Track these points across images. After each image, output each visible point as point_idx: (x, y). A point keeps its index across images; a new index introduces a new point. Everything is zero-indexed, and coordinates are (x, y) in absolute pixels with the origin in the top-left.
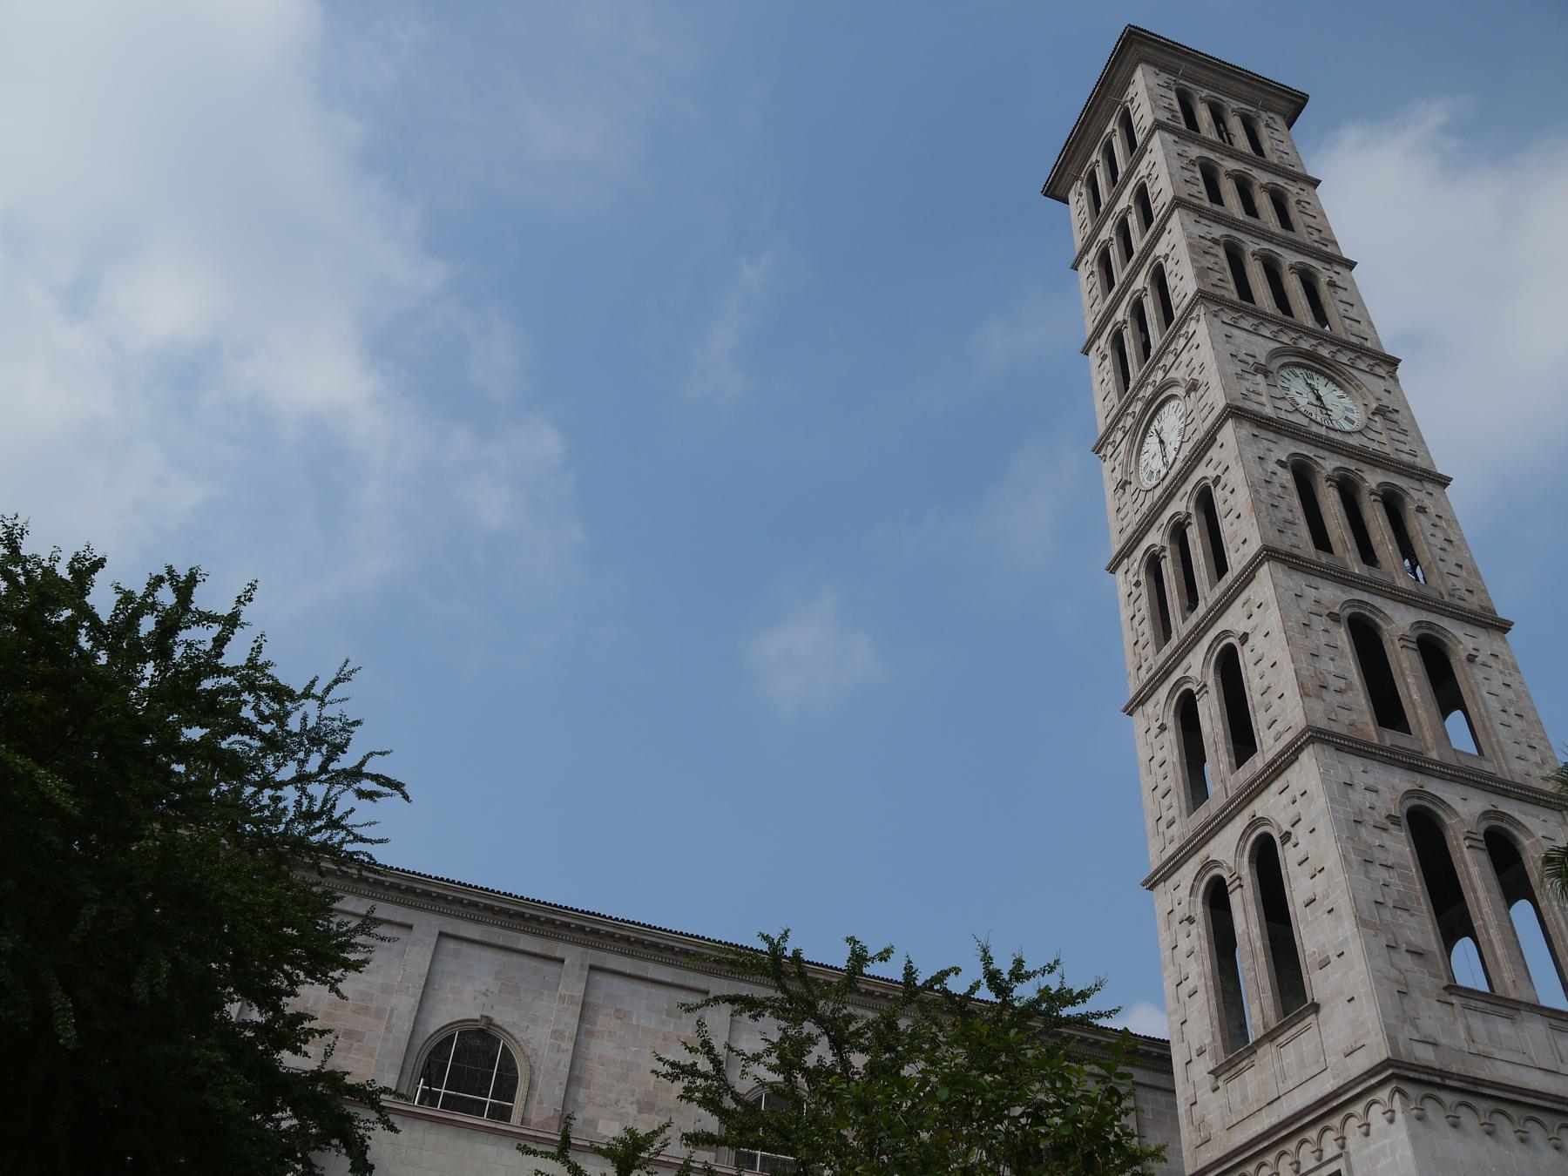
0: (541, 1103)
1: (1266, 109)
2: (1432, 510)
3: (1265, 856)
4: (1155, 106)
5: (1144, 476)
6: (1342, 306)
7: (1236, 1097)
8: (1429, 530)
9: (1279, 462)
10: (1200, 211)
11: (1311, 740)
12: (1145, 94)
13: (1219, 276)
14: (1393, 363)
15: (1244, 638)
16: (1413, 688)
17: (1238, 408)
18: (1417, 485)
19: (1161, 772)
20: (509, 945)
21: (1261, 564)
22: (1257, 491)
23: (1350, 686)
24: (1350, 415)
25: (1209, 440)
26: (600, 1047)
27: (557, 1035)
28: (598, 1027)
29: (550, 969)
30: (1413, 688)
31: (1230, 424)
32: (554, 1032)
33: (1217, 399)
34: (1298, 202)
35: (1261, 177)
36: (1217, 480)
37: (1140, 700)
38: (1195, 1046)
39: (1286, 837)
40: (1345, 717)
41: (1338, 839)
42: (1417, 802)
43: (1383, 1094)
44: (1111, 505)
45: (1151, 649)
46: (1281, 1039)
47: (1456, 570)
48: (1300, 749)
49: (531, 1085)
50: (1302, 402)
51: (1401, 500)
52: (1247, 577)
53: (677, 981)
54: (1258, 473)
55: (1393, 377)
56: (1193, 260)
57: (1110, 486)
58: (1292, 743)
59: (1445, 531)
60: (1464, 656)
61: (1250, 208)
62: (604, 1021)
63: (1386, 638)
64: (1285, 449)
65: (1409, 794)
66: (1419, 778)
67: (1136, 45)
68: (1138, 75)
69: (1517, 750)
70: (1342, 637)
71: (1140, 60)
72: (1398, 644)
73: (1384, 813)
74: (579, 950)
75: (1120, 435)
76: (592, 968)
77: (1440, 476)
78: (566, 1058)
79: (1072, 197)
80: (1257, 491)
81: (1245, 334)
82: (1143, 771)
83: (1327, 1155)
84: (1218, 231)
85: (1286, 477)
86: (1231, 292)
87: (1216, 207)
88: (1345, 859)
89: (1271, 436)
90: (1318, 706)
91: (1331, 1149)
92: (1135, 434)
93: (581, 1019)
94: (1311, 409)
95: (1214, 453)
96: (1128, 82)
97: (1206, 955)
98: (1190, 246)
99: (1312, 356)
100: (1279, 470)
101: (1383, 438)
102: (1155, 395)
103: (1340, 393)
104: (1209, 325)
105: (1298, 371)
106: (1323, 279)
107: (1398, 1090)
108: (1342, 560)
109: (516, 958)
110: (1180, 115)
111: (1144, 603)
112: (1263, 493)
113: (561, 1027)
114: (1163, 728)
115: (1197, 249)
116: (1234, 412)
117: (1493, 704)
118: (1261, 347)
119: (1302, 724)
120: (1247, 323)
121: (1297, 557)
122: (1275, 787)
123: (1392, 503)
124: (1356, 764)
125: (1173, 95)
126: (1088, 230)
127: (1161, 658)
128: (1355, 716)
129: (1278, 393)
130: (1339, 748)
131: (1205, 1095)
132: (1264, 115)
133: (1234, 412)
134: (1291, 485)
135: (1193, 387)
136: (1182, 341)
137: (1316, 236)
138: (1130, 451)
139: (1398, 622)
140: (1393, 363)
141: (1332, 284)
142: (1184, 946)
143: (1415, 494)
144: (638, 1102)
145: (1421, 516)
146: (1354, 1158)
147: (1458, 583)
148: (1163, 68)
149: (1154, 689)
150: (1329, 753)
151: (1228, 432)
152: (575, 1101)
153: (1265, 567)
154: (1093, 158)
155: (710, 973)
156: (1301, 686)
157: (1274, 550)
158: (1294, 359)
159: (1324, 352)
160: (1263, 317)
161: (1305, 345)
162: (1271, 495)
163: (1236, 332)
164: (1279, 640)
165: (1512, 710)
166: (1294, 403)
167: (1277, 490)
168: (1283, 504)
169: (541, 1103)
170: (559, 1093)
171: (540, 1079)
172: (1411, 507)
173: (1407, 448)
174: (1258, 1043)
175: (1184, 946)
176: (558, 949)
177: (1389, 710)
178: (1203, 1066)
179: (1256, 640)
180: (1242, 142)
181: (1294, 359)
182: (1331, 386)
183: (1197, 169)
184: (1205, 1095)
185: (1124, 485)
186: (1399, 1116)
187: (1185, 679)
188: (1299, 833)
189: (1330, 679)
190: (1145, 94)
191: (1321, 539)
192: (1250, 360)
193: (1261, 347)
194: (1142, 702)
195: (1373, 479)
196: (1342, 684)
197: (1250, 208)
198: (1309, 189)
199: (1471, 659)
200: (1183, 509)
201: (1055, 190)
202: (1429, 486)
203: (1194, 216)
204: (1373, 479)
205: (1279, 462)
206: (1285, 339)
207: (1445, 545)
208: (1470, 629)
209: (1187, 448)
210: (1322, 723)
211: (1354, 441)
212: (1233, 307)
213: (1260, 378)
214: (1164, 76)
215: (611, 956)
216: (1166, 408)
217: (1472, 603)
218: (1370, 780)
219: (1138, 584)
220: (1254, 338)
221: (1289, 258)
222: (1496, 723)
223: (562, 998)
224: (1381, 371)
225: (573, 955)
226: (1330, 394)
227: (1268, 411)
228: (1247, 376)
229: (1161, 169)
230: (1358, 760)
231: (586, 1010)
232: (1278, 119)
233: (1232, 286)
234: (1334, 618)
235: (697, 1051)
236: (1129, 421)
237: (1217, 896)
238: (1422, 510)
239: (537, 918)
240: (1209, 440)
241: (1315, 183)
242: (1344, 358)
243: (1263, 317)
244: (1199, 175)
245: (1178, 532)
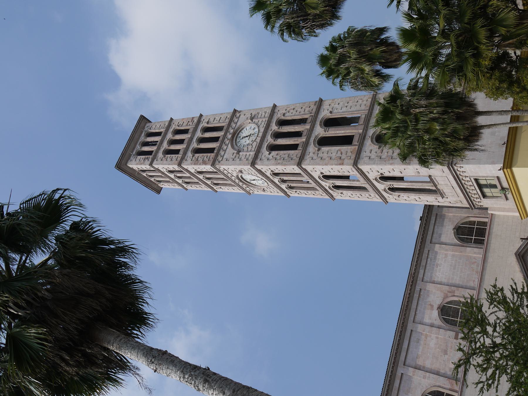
0: (445, 384)
1: (144, 128)
2: (284, 111)
3: (384, 178)
4: (143, 164)
5: (263, 185)
6: (215, 121)
7: (450, 194)
8: (290, 114)
9: (269, 154)
10: (183, 159)
11: (356, 166)
12: (135, 165)
13: (205, 158)
14: (235, 111)
15: (322, 173)
16: (340, 132)
17: (252, 163)
18: (276, 114)
19: (354, 195)
20: (397, 390)
21: (302, 167)
22: (279, 163)
23: (340, 150)
24: (252, 128)
25: (260, 172)
26: (428, 364)
27: (424, 377)
28: (422, 365)
29: (404, 377)
30: (340, 132)
31: (256, 166)
32: (424, 378)
33: (247, 168)
34: (178, 126)
35: (169, 136)
36: (272, 171)
37: (332, 196)
38: (435, 200)
39: (381, 174)
40: (349, 154)
41: (385, 165)
42: (374, 139)
43: (455, 168)
44: (269, 193)
45: (317, 192)
46: (437, 184)
47: (303, 110)
48: (358, 168)
49: (440, 387)
50: (248, 142)
51: (281, 120)
52: (305, 171)
53: (408, 339)
54: (273, 161)
55: (240, 112)
56: (200, 164)
57: (263, 193)
58: (356, 170)
59: (291, 109)
60: (330, 114)
61: (181, 142)
62: (420, 362)
63: (324, 136)
64: (265, 151)
65: (372, 141)
66: (367, 137)
67: (121, 165)
68: (131, 166)
69: (358, 106)
70: (325, 149)
71: (126, 165)
72: (327, 133)
73: (377, 149)
74: (399, 368)
75: (248, 188)
76: (404, 365)
77: (273, 107)
78: (432, 375)
79: (161, 186)
80: (279, 163)
81: (226, 154)
82: (353, 199)
83: (469, 180)
84: (189, 154)
85: (274, 153)
86: (212, 155)
87: (162, 134)
88: (391, 164)
89: (260, 154)
90: (346, 161)
91: (468, 179)
92: (249, 185)
93: (419, 369)
94: (251, 139)
95: (263, 171)
96: (132, 169)
97: (410, 194)
98: (195, 164)
99: (234, 135)
100: (271, 155)
101: (261, 120)
102: (241, 181)
103: (245, 129)
104: (223, 165)
105: (238, 141)
106: (206, 125)
107: (455, 165)
108: (301, 142)
109: (401, 388)
110: (146, 156)
111: (301, 191)
112: (279, 161)
113: (422, 376)
114: (342, 193)
115: (196, 162)
116: (253, 164)
117: (344, 109)
118: (230, 151)
119: (351, 167)
120: (222, 153)
121: (300, 157)
122: (367, 174)
123: (282, 123)
124: (363, 154)
125: (139, 157)
126: (176, 184)
127: (320, 190)
128: (349, 151)
129: (245, 149)
130: (359, 158)
131: (448, 200)
132: (146, 129)
133: (253, 164)
134: (276, 152)
135: (241, 171)
136: (225, 171)
137: (191, 123)
138: (254, 187)
139: (320, 131)
140: (235, 111)
141: (208, 123)
142: (405, 198)
143: (278, 115)
144: (444, 355)
145: (286, 115)
146: (471, 175)
147: (307, 109)
148: (129, 159)
149: (329, 193)
150: (361, 161)
151: (258, 167)
152: (444, 374)
153: (303, 166)
154: (145, 175)
155: (406, 329)
156: (340, 164)
157: (298, 163)
158: (234, 141)
159: (232, 131)
160: (220, 148)
161: (229, 136)
162: (280, 159)
163: (225, 157)
164: (322, 164)
165: (346, 104)
166: (248, 144)
167: (278, 157)
168: (284, 156)
169: (445, 384)
170: (442, 378)
171: (438, 384)
172: (283, 118)
173: (264, 114)
174: (437, 188)
175: (405, 198)
176: (399, 374)
177: (347, 140)
178: (440, 199)
179: (323, 171)
180: (157, 139)
181: (234, 141)
182: (243, 131)
183: (167, 156)
184: (448, 200)
185: (264, 190)
186: (461, 166)
187: (330, 188)
188: (381, 171)
189: (337, 155)
190: (135, 165)
191: (294, 147)
192: (235, 155)
193: (230, 151)
194: (332, 196)
195: (274, 127)
196: (339, 152)
197: (181, 142)
198: (173, 121)
199: (331, 112)
200: (277, 180)
201: (158, 190)
202: (276, 110)
203: (184, 161)
204: (274, 127)
205: (269, 154)
206: (227, 142)
207: (295, 110)
208: (322, 110)
209: (259, 175)
210: (352, 162)
211: (262, 130)
212: (217, 155)
213: (241, 153)
214: (131, 158)
215: (401, 358)
216: (244, 177)
217: (314, 108)
218: (368, 151)
219: (296, 192)
220: (227, 152)
221: (199, 134)
222: (350, 110)
223: (414, 375)
224: (238, 115)
225: (400, 370)
226: (245, 133)
227: (252, 154)
228: (240, 157)
229: (165, 166)
230: (362, 153)
231: (417, 368)
232: (147, 125)
233: (209, 154)
234: (319, 150)
235: (457, 371)
236: (244, 186)
237: (393, 190)
238: (284, 115)
239: (390, 380)
240: (260, 172)
241: (172, 119)
242: (233, 125)
243: (220, 148)
244: (169, 156)
245: (284, 181)
